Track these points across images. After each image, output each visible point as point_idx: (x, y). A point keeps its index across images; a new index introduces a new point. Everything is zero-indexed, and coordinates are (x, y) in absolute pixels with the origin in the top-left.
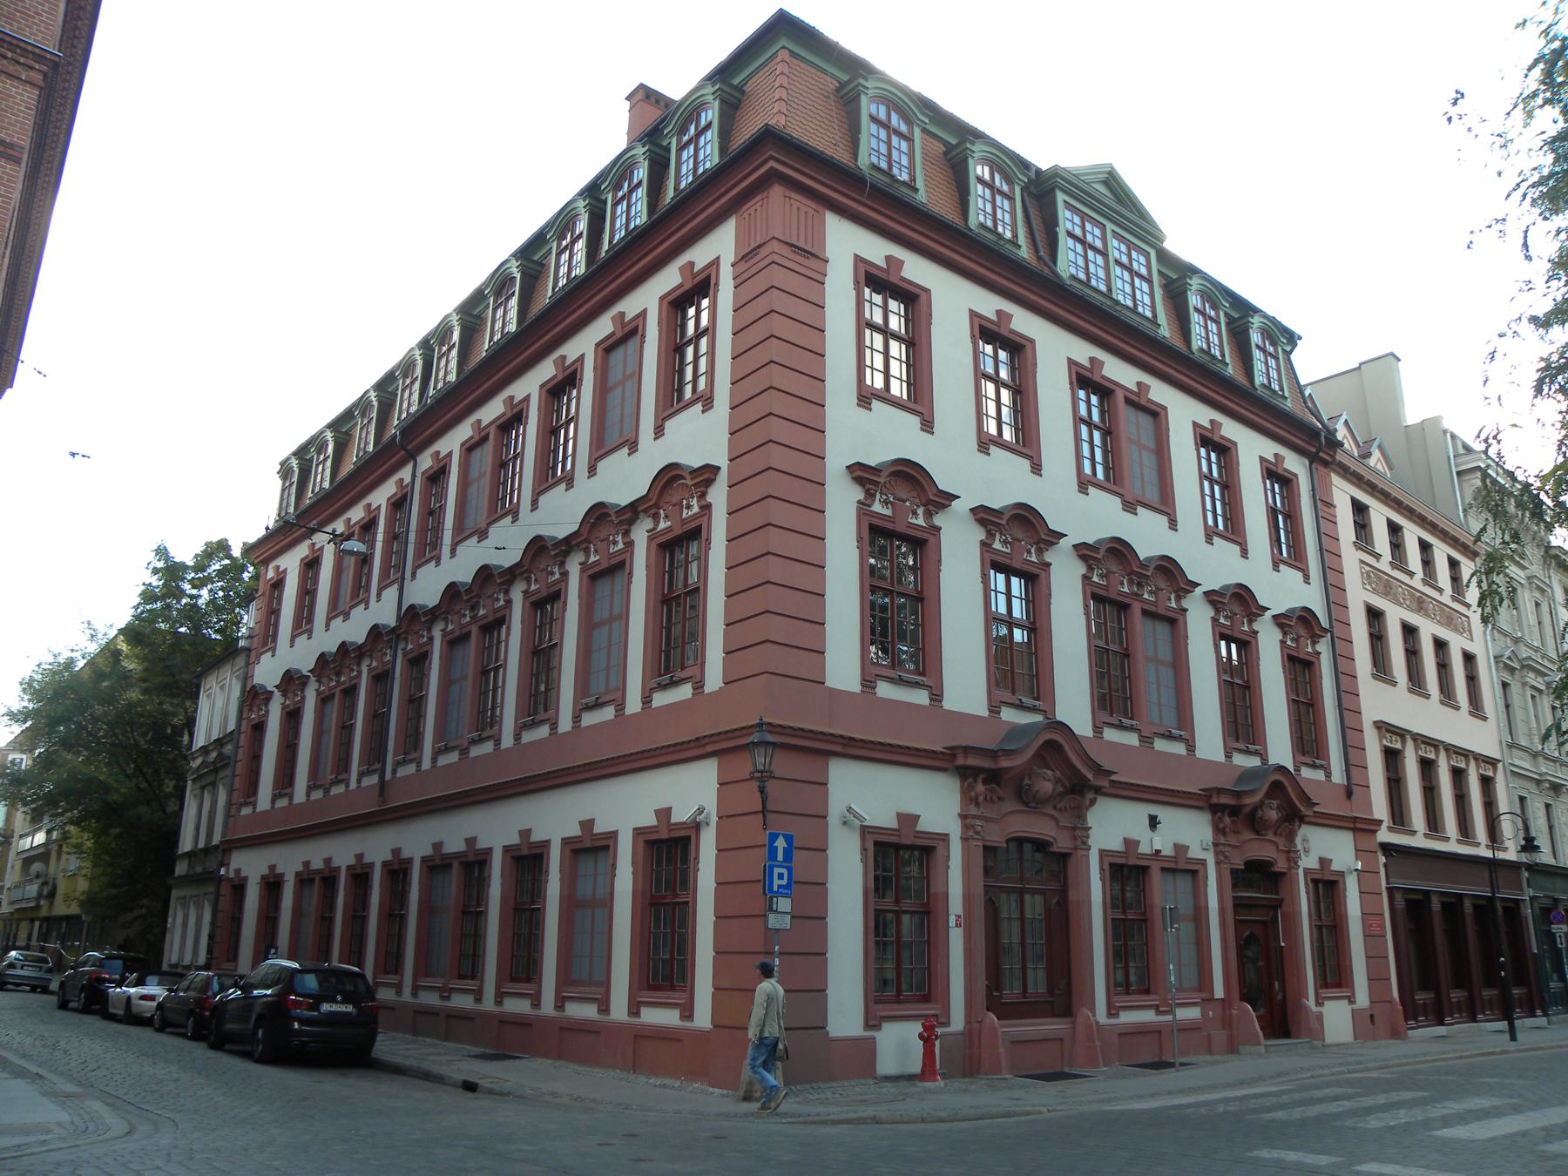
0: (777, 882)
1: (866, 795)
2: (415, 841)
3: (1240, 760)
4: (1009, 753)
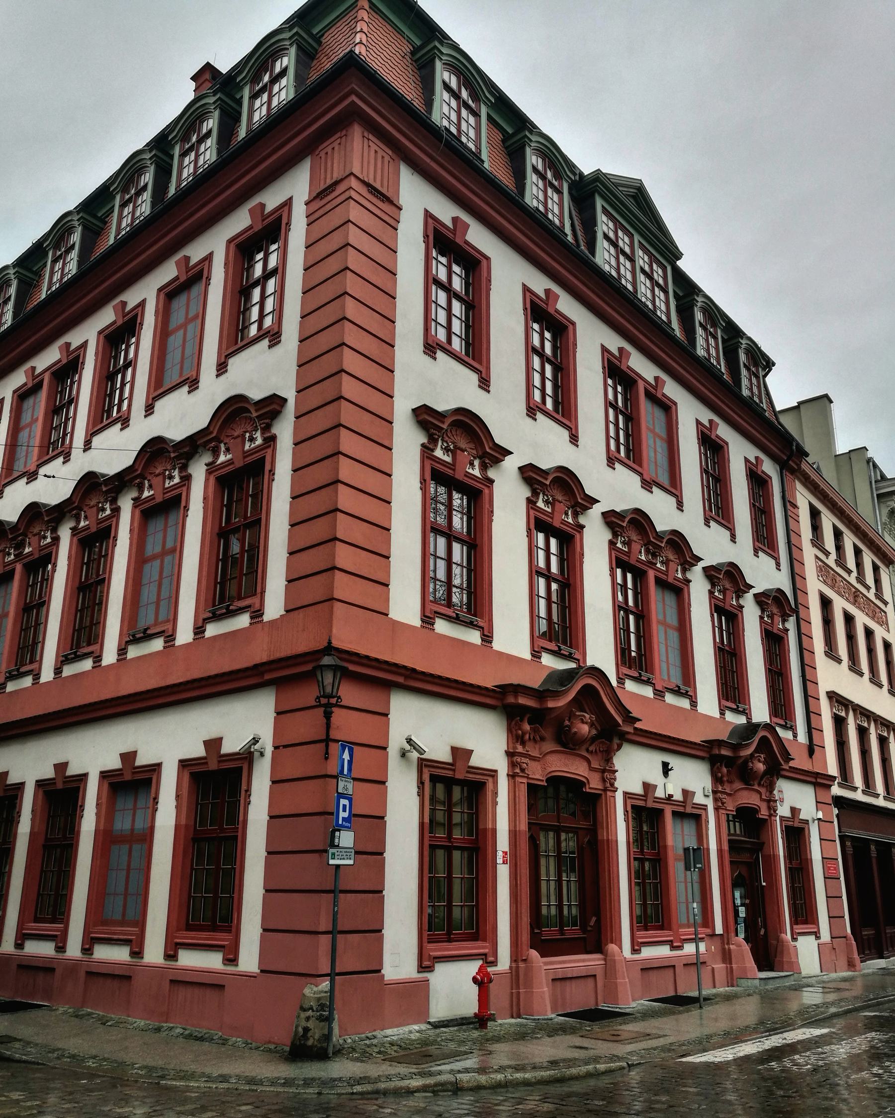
1: (425, 727)
3: (730, 717)
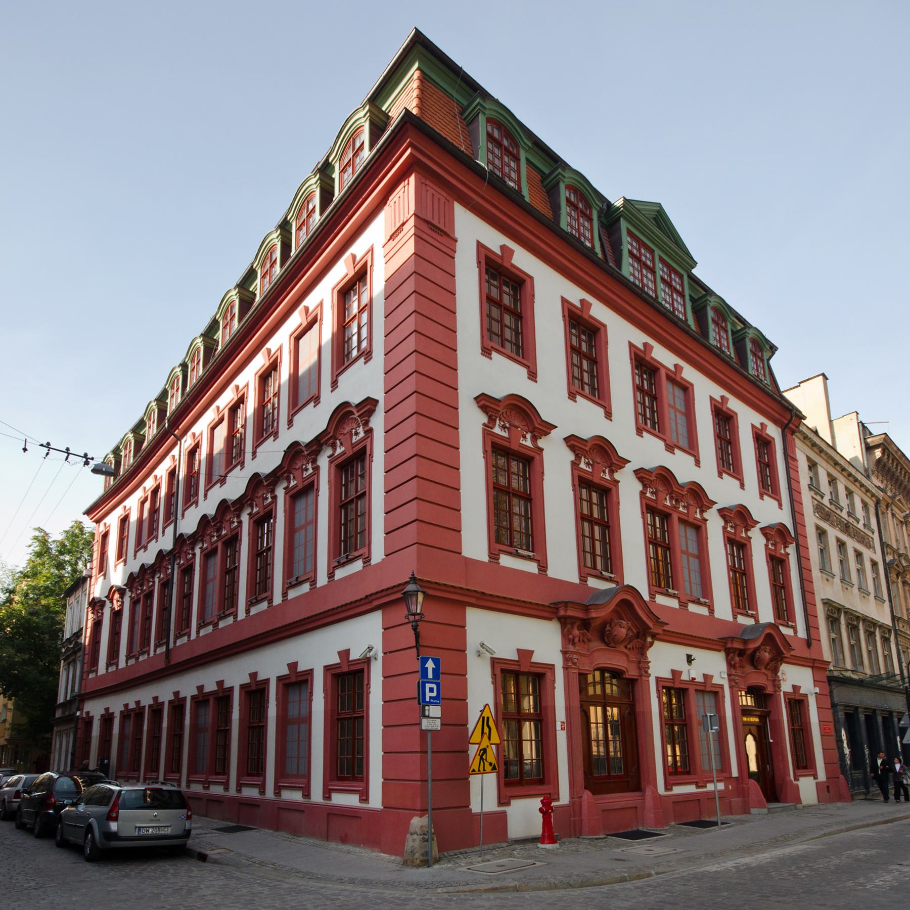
0: (428, 694)
1: (494, 635)
2: (187, 685)
3: (742, 620)
4: (597, 606)
